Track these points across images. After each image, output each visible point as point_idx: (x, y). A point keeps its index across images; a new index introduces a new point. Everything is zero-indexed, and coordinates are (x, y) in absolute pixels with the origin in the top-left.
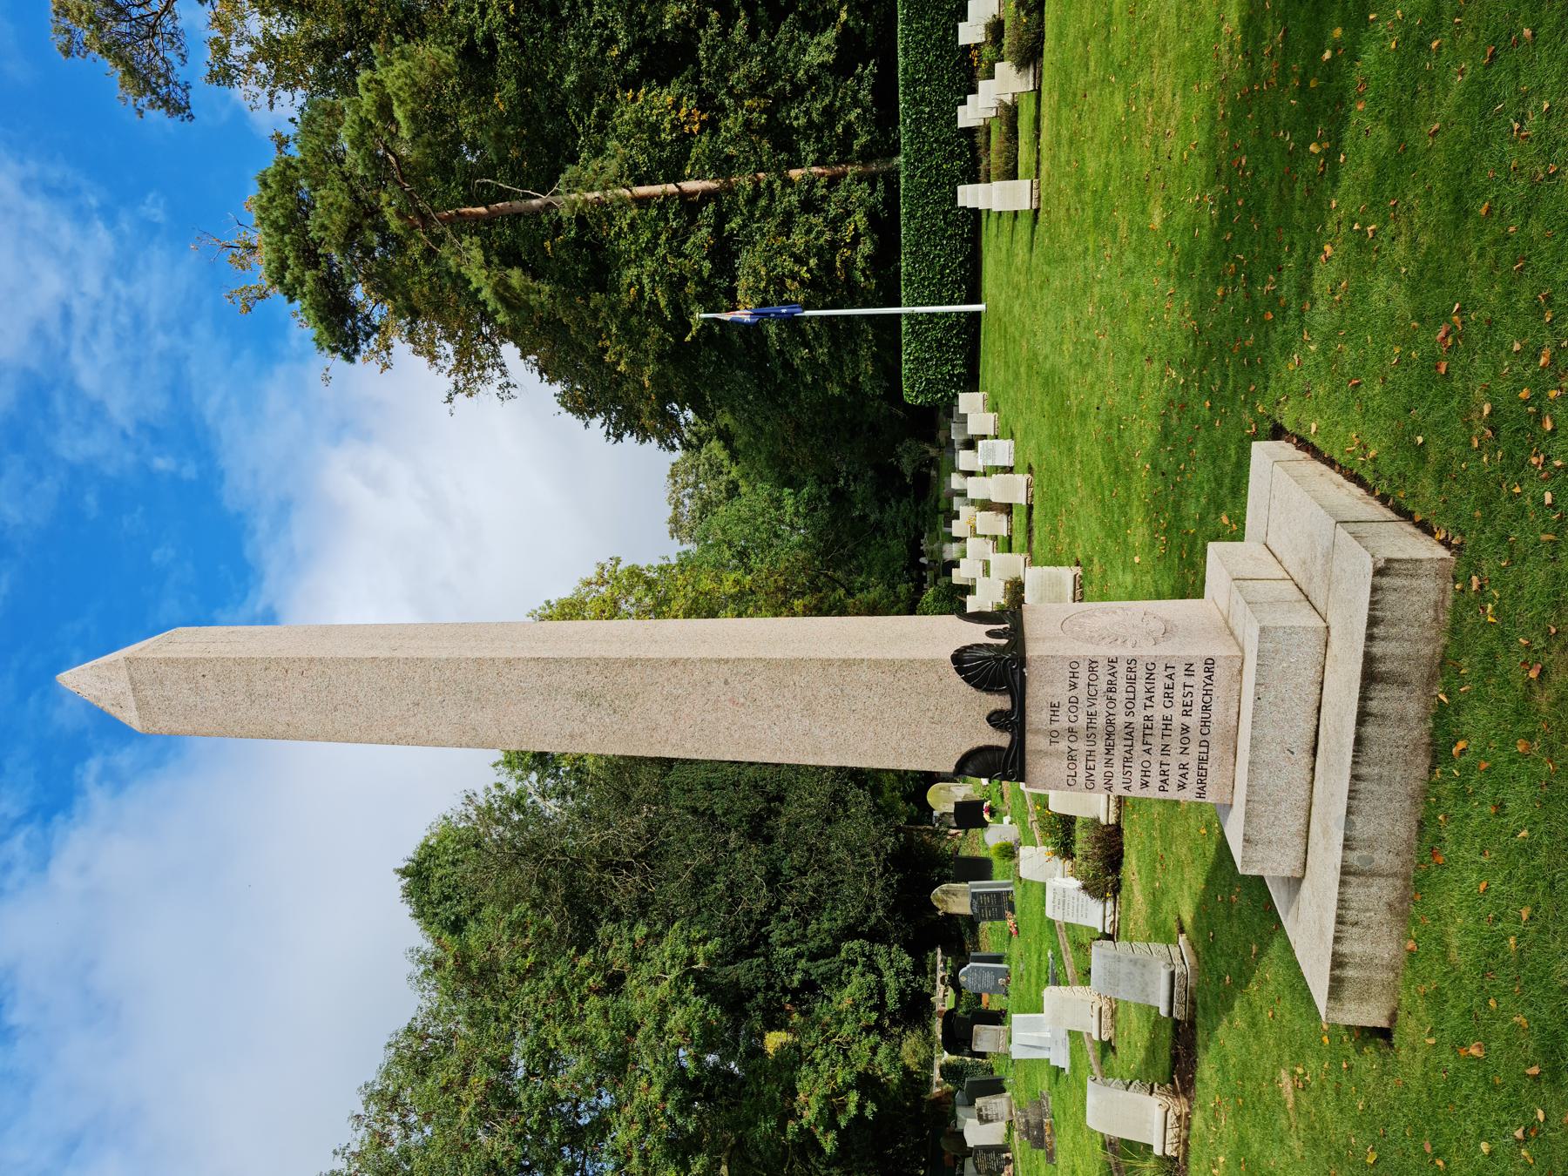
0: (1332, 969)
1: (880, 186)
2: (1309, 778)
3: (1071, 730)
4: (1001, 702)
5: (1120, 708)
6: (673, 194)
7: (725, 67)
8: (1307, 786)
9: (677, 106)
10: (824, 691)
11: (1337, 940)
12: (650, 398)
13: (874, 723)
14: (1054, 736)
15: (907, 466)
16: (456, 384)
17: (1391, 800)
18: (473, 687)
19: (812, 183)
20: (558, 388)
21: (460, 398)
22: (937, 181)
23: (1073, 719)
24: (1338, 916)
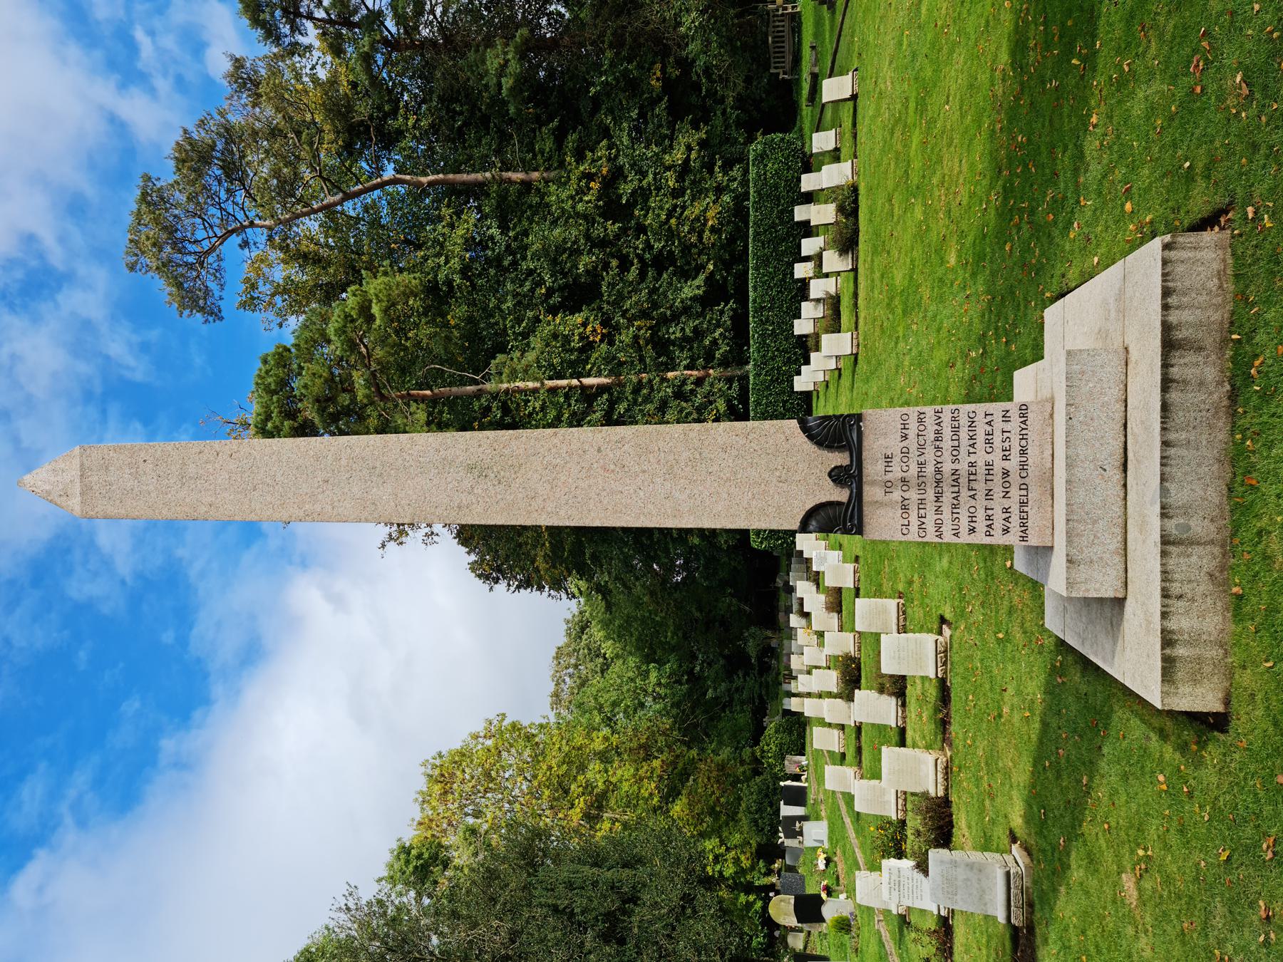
0: (1163, 648)
1: (735, 384)
2: (1122, 495)
3: (904, 480)
4: (840, 459)
5: (947, 457)
6: (576, 387)
7: (621, 297)
8: (1121, 503)
9: (585, 325)
10: (685, 455)
11: (1164, 615)
12: (544, 544)
13: (728, 484)
14: (888, 486)
15: (752, 649)
16: (390, 535)
17: (1199, 465)
18: (378, 464)
19: (684, 382)
20: (473, 557)
21: (392, 546)
22: (777, 379)
23: (905, 468)
24: (1163, 589)
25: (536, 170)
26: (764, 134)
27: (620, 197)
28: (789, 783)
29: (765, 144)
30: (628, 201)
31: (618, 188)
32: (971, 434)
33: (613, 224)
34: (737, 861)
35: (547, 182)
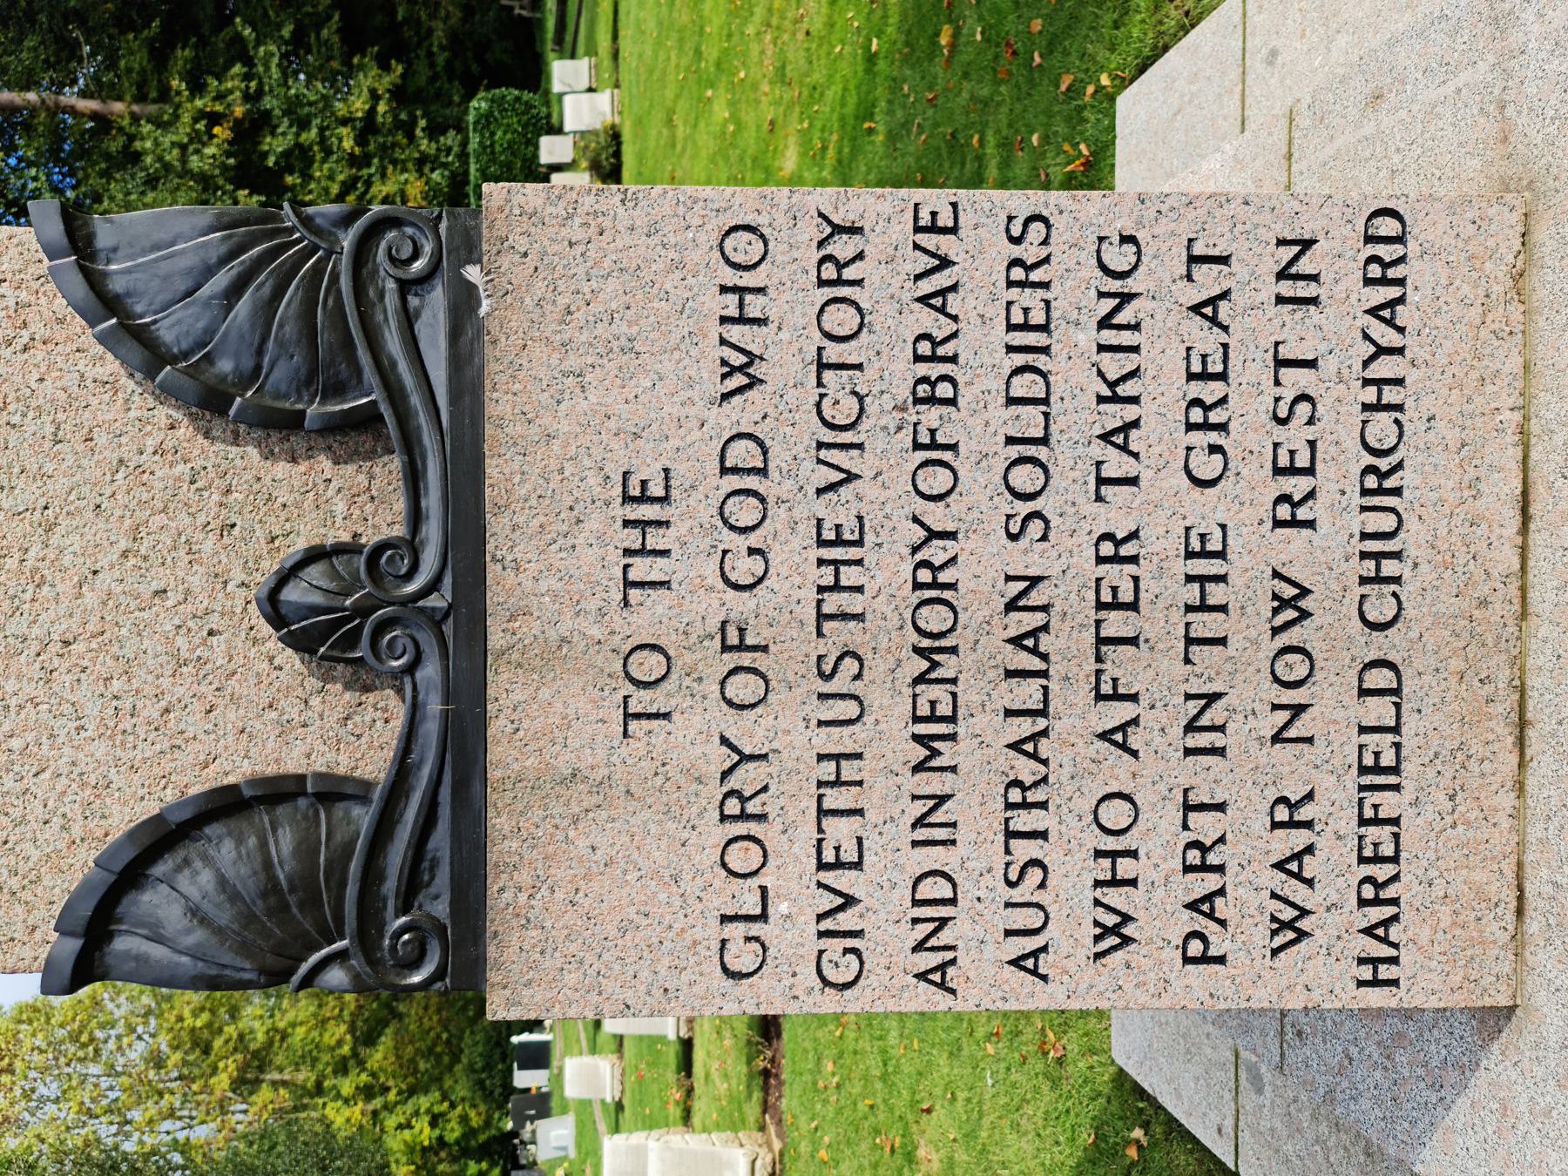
25: (119, 98)
26: (488, 89)
27: (265, 155)
28: (525, 1037)
29: (492, 101)
30: (276, 163)
31: (260, 143)
32: (1114, 366)
33: (250, 194)
34: (464, 1119)
35: (135, 119)
